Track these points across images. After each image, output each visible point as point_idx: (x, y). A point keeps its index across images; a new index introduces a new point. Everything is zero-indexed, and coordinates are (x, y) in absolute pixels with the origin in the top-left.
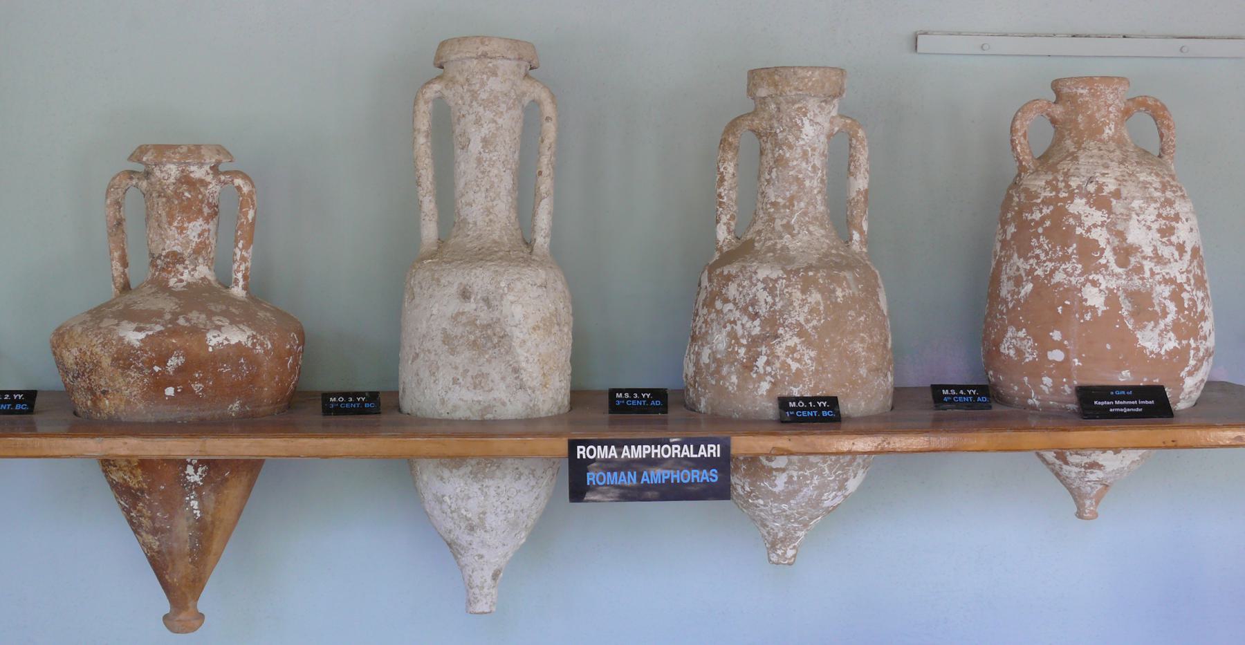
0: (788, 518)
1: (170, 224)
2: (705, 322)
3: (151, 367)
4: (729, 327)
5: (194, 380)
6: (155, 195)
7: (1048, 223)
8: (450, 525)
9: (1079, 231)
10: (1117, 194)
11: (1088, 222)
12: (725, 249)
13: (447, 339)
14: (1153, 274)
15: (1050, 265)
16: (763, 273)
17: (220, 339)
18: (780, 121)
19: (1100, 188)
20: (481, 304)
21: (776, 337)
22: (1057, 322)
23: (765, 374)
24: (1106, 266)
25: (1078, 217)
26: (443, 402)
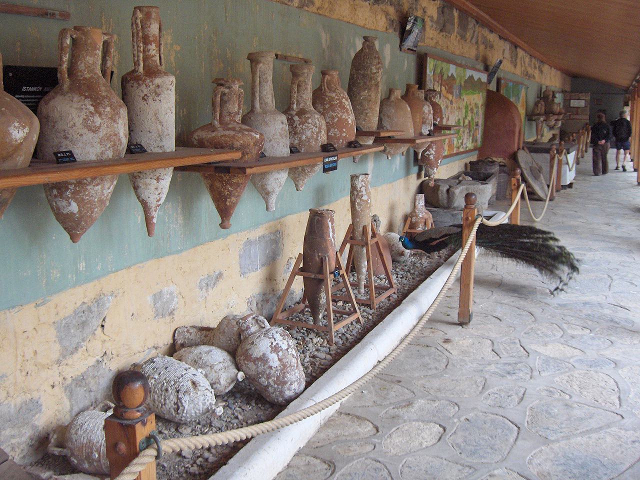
2: (302, 129)
13: (281, 135)
15: (341, 114)
22: (344, 127)
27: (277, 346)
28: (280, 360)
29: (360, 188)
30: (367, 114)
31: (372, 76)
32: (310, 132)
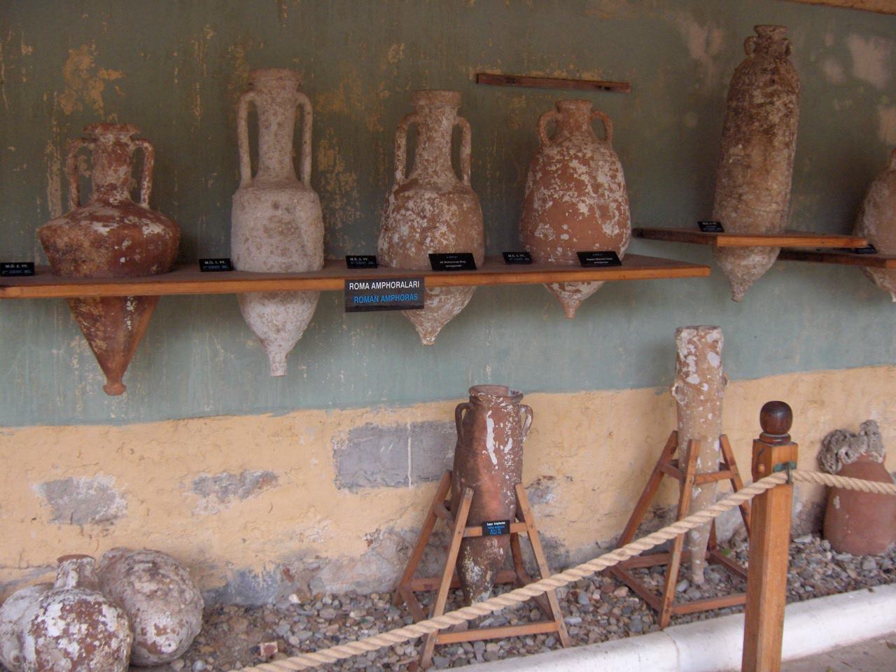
0: (436, 320)
1: (110, 168)
3: (113, 247)
4: (410, 223)
5: (135, 253)
6: (100, 151)
7: (560, 172)
8: (266, 329)
9: (575, 176)
10: (592, 158)
11: (580, 171)
12: (401, 184)
13: (266, 230)
14: (609, 197)
15: (561, 193)
16: (428, 195)
17: (149, 231)
18: (431, 118)
19: (584, 155)
20: (285, 211)
21: (435, 228)
23: (431, 246)
24: (588, 193)
25: (574, 169)
26: (265, 263)
27: (42, 626)
28: (38, 652)
29: (685, 357)
30: (741, 195)
31: (754, 111)
32: (407, 226)
